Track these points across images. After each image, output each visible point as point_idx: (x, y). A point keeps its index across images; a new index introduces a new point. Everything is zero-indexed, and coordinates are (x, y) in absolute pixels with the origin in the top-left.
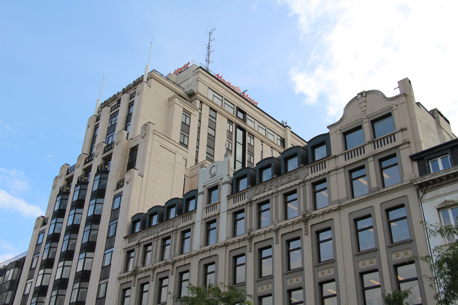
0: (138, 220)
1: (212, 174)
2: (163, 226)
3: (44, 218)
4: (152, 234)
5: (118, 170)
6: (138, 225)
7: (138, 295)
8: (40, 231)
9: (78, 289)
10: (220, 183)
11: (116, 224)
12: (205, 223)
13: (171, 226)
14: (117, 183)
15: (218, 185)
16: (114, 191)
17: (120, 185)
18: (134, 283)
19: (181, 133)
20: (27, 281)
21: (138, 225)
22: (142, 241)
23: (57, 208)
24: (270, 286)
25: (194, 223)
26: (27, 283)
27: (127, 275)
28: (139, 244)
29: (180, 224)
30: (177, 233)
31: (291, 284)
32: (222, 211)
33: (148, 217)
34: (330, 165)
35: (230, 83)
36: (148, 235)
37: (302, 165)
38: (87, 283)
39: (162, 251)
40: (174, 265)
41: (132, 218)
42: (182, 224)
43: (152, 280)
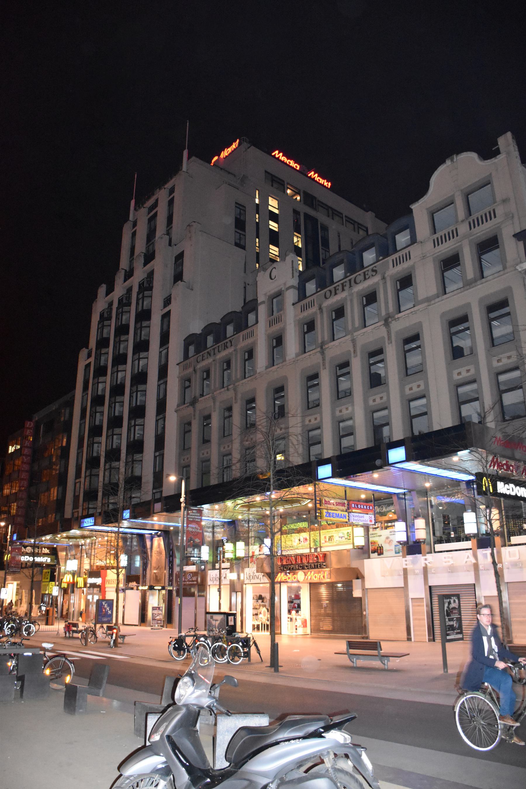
6: (192, 349)
11: (166, 350)
17: (167, 301)
19: (236, 231)
21: (192, 349)
24: (350, 409)
31: (374, 404)
34: (415, 251)
35: (333, 219)
37: (381, 258)
41: (184, 340)
42: (243, 344)
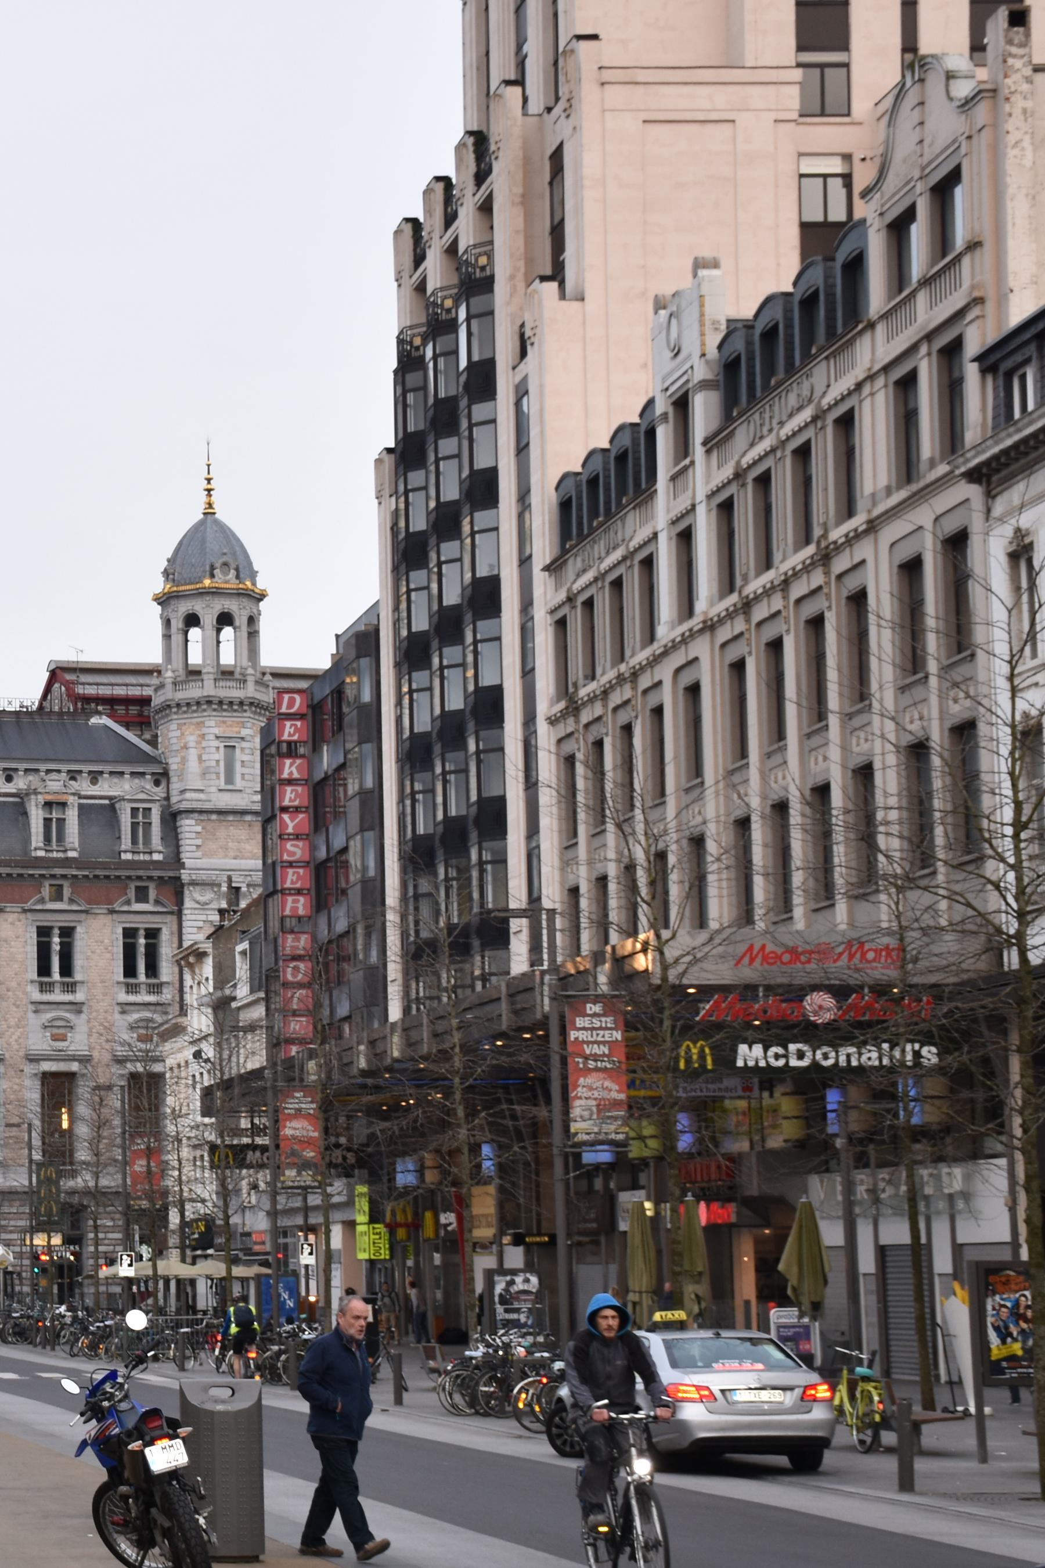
10: (690, 385)
15: (686, 394)
16: (510, 371)
25: (655, 535)
30: (631, 566)
41: (557, 488)
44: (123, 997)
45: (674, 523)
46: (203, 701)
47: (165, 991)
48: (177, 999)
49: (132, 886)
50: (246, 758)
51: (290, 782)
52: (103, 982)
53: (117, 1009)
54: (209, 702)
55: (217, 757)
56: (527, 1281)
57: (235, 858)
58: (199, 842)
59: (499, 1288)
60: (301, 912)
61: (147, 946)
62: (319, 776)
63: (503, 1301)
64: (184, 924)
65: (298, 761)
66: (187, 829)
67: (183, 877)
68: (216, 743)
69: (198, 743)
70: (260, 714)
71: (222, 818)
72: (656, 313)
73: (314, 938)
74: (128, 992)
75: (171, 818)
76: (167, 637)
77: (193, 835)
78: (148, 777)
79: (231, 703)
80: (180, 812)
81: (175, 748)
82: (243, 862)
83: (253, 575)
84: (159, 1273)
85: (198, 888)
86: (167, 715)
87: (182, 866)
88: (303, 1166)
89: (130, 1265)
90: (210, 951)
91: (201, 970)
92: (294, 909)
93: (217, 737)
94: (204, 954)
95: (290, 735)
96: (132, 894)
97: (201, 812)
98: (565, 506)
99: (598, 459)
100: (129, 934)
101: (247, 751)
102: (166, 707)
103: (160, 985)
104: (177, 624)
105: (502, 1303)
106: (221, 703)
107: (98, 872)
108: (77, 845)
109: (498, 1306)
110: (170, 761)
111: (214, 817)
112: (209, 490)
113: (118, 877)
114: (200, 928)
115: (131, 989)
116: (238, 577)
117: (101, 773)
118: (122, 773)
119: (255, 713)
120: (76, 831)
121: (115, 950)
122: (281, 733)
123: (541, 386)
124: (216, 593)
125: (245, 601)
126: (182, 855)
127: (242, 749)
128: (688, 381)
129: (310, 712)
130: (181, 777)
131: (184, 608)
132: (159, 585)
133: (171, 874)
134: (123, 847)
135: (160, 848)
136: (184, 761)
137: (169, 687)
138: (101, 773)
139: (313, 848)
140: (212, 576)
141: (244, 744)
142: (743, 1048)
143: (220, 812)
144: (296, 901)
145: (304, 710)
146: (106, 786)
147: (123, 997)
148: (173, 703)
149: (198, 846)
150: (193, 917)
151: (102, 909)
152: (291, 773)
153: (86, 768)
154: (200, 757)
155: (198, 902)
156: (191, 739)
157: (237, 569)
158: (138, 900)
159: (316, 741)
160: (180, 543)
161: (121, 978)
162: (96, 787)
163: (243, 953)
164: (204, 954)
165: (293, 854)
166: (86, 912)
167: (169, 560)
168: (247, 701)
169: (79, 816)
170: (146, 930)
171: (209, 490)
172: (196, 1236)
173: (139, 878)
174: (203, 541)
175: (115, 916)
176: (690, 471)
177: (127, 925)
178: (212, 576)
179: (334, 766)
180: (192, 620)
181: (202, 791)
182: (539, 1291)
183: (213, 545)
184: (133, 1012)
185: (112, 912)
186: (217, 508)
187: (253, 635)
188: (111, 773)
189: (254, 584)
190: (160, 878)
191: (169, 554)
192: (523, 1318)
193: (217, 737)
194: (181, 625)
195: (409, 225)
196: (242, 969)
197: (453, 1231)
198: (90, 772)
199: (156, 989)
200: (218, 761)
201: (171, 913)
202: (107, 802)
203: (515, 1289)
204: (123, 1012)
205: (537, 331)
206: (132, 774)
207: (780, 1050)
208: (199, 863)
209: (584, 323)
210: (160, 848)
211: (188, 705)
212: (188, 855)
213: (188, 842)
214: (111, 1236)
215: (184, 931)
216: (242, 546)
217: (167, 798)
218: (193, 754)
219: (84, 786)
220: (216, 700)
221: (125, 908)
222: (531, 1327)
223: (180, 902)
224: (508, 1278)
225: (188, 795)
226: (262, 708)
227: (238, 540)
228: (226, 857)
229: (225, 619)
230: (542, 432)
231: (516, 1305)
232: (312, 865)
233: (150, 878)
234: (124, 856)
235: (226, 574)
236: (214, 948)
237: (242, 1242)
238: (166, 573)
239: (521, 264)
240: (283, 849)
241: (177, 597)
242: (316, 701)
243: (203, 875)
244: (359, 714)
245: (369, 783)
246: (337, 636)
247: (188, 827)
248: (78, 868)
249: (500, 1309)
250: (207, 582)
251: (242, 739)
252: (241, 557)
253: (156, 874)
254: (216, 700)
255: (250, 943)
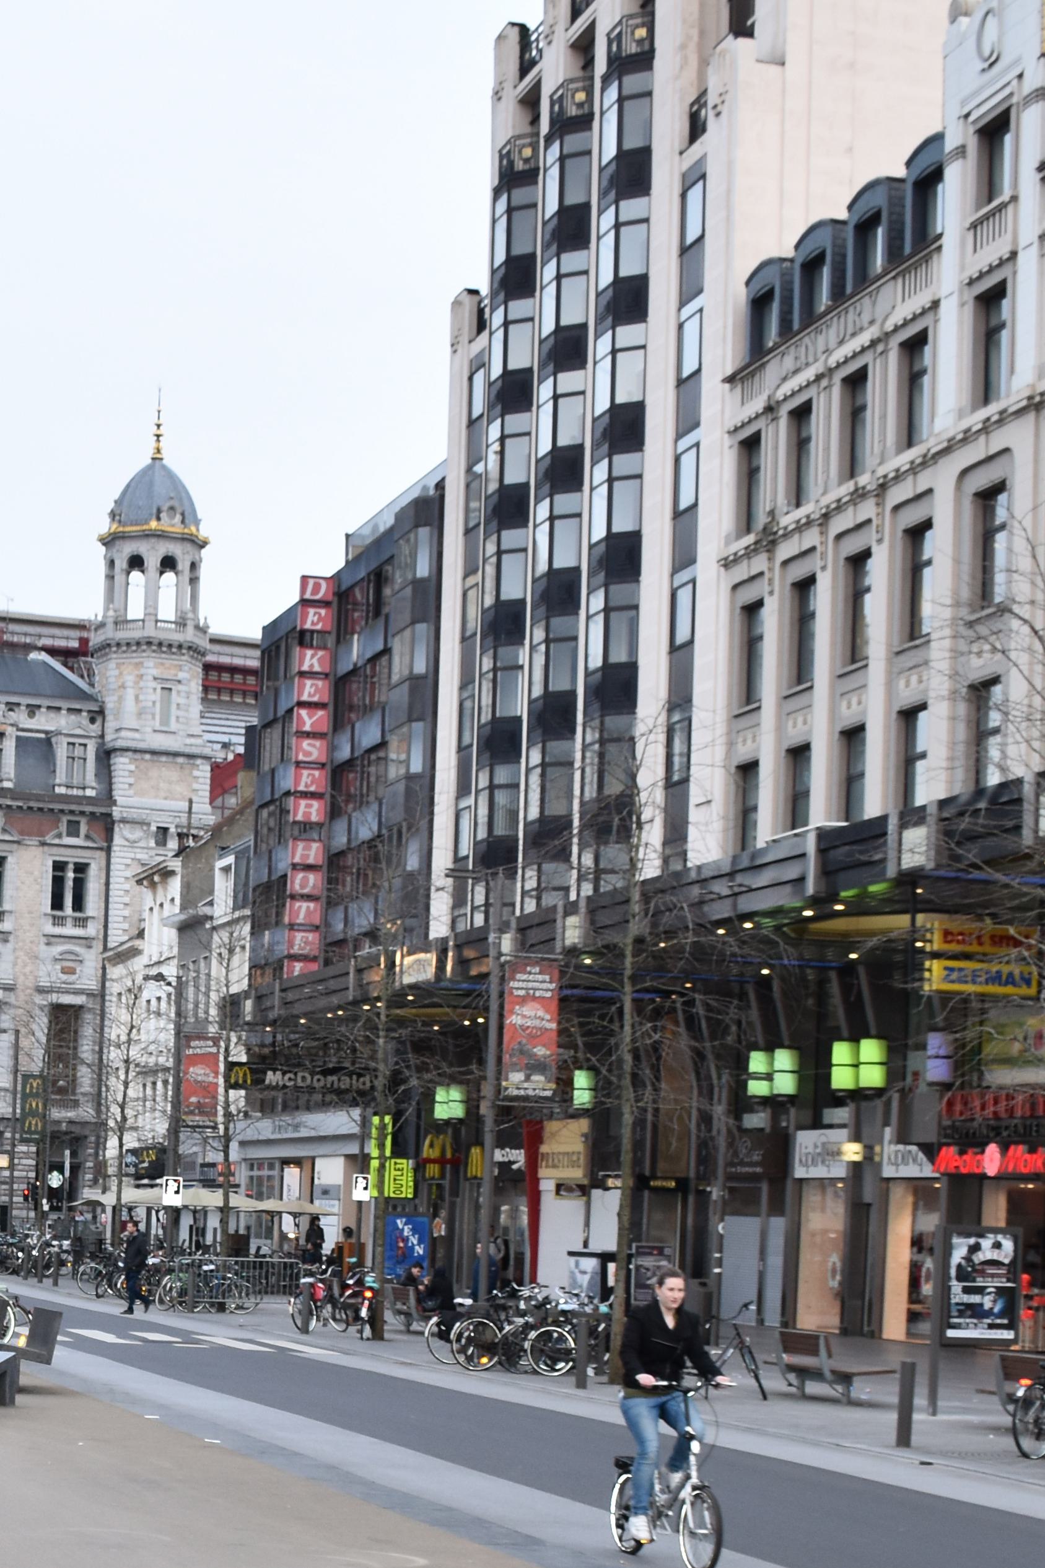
0: (872, 216)
1: (987, 53)
2: (842, 320)
3: (476, 298)
4: (811, 359)
5: (683, 47)
7: (841, 606)
8: (471, 361)
9: (602, 615)
10: (1014, 100)
12: (736, 446)
13: (866, 318)
14: (687, 109)
15: (1007, 112)
16: (677, 157)
18: (771, 581)
20: (676, 441)
22: (780, 395)
23: (501, 257)
25: (936, 304)
26: (679, 451)
27: (746, 548)
28: (770, 409)
29: (894, 307)
30: (829, 387)
32: (1022, 243)
33: (850, 234)
36: (798, 365)
38: (634, 585)
39: (849, 440)
40: (884, 500)
41: (748, 283)
43: (880, 541)
44: (50, 929)
45: (971, 282)
46: (143, 641)
47: (90, 924)
48: (101, 937)
49: (65, 819)
50: (182, 701)
51: (311, 674)
52: (30, 912)
53: (44, 940)
54: (149, 643)
55: (153, 697)
56: (997, 1245)
57: (166, 798)
58: (131, 780)
59: (958, 1256)
60: (314, 818)
61: (75, 880)
62: (344, 667)
63: (962, 1275)
64: (113, 860)
65: (320, 653)
66: (121, 766)
67: (114, 814)
68: (153, 684)
69: (136, 683)
70: (197, 659)
71: (155, 758)
72: (953, 20)
73: (327, 849)
74: (54, 924)
75: (105, 755)
76: (110, 577)
77: (127, 774)
78: (84, 714)
79: (170, 646)
80: (115, 750)
81: (112, 686)
82: (172, 802)
83: (197, 522)
84: (123, 1202)
85: (128, 826)
86: (106, 654)
87: (114, 803)
88: (535, 1067)
89: (177, 1192)
90: (178, 870)
91: (165, 889)
92: (307, 814)
93: (155, 679)
94: (172, 873)
95: (313, 623)
96: (63, 827)
97: (135, 751)
98: (759, 304)
99: (774, 270)
100: (59, 867)
101: (183, 694)
102: (106, 646)
103: (86, 919)
104: (121, 564)
105: (959, 1278)
106: (160, 644)
107: (32, 804)
108: (12, 776)
109: (954, 1282)
110: (107, 700)
111: (148, 757)
112: (158, 436)
113: (52, 810)
114: (127, 865)
115: (58, 921)
116: (183, 522)
117: (39, 707)
118: (59, 709)
119: (192, 657)
120: (13, 761)
121: (44, 882)
122: (304, 621)
123: (730, 165)
124: (161, 535)
125: (188, 547)
126: (114, 793)
127: (179, 692)
128: (1011, 94)
129: (336, 600)
130: (117, 715)
131: (128, 549)
132: (105, 526)
133: (103, 810)
134: (58, 781)
135: (94, 784)
136: (121, 699)
137: (110, 626)
138: (39, 707)
139: (332, 748)
140: (158, 519)
141: (180, 687)
142: (270, 1073)
143: (154, 753)
144: (309, 806)
145: (330, 598)
146: (43, 719)
147: (50, 929)
148: (113, 643)
149: (130, 785)
150: (122, 854)
151: (34, 841)
152: (312, 666)
153: (25, 701)
154: (137, 697)
155: (127, 840)
156: (129, 679)
157: (183, 514)
158: (69, 834)
159: (342, 631)
160: (128, 486)
161: (48, 910)
162: (34, 721)
163: (226, 870)
164: (172, 873)
165: (309, 754)
166: (18, 842)
167: (116, 502)
168: (186, 645)
169: (17, 747)
170: (75, 864)
171: (158, 436)
172: (146, 1165)
173: (72, 812)
174: (151, 484)
175: (46, 848)
176: (1010, 208)
177: (58, 859)
178: (158, 519)
179: (369, 655)
180: (136, 562)
181: (137, 730)
182: (1013, 1262)
183: (161, 489)
184: (57, 944)
185: (43, 844)
186: (165, 454)
187: (194, 581)
188: (49, 708)
189: (198, 530)
190: (92, 814)
191: (117, 496)
192: (987, 1302)
193: (155, 679)
194: (125, 565)
195: (516, 30)
196: (223, 889)
197: (519, 1170)
198: (28, 706)
199: (82, 922)
200: (154, 703)
201: (101, 849)
202: (43, 736)
203: (979, 1257)
204: (48, 944)
205: (727, 97)
206: (69, 710)
207: (292, 1076)
208: (135, 801)
209: (784, 91)
210: (94, 784)
211: (128, 644)
212: (121, 792)
213: (121, 779)
214: (24, 1161)
215: (112, 867)
216: (187, 493)
217: (102, 736)
218: (130, 694)
219: (21, 717)
220: (156, 642)
221: (56, 841)
222: (1001, 1315)
223: (109, 838)
224: (972, 1241)
225: (123, 734)
226: (199, 653)
227: (184, 487)
228: (156, 797)
229: (168, 563)
230: (728, 220)
231: (980, 1282)
232: (328, 768)
233: (82, 813)
234: (58, 790)
235: (172, 517)
236: (183, 866)
237: (202, 1173)
238: (113, 515)
239: (695, 33)
240: (299, 748)
241: (123, 538)
242: (344, 588)
243: (133, 814)
244: (414, 591)
245: (420, 667)
246: (348, 536)
247: (122, 765)
248: (13, 799)
249: (956, 1287)
250: (154, 524)
251: (179, 682)
252: (186, 502)
253: (88, 809)
254: (156, 642)
255: (236, 858)
